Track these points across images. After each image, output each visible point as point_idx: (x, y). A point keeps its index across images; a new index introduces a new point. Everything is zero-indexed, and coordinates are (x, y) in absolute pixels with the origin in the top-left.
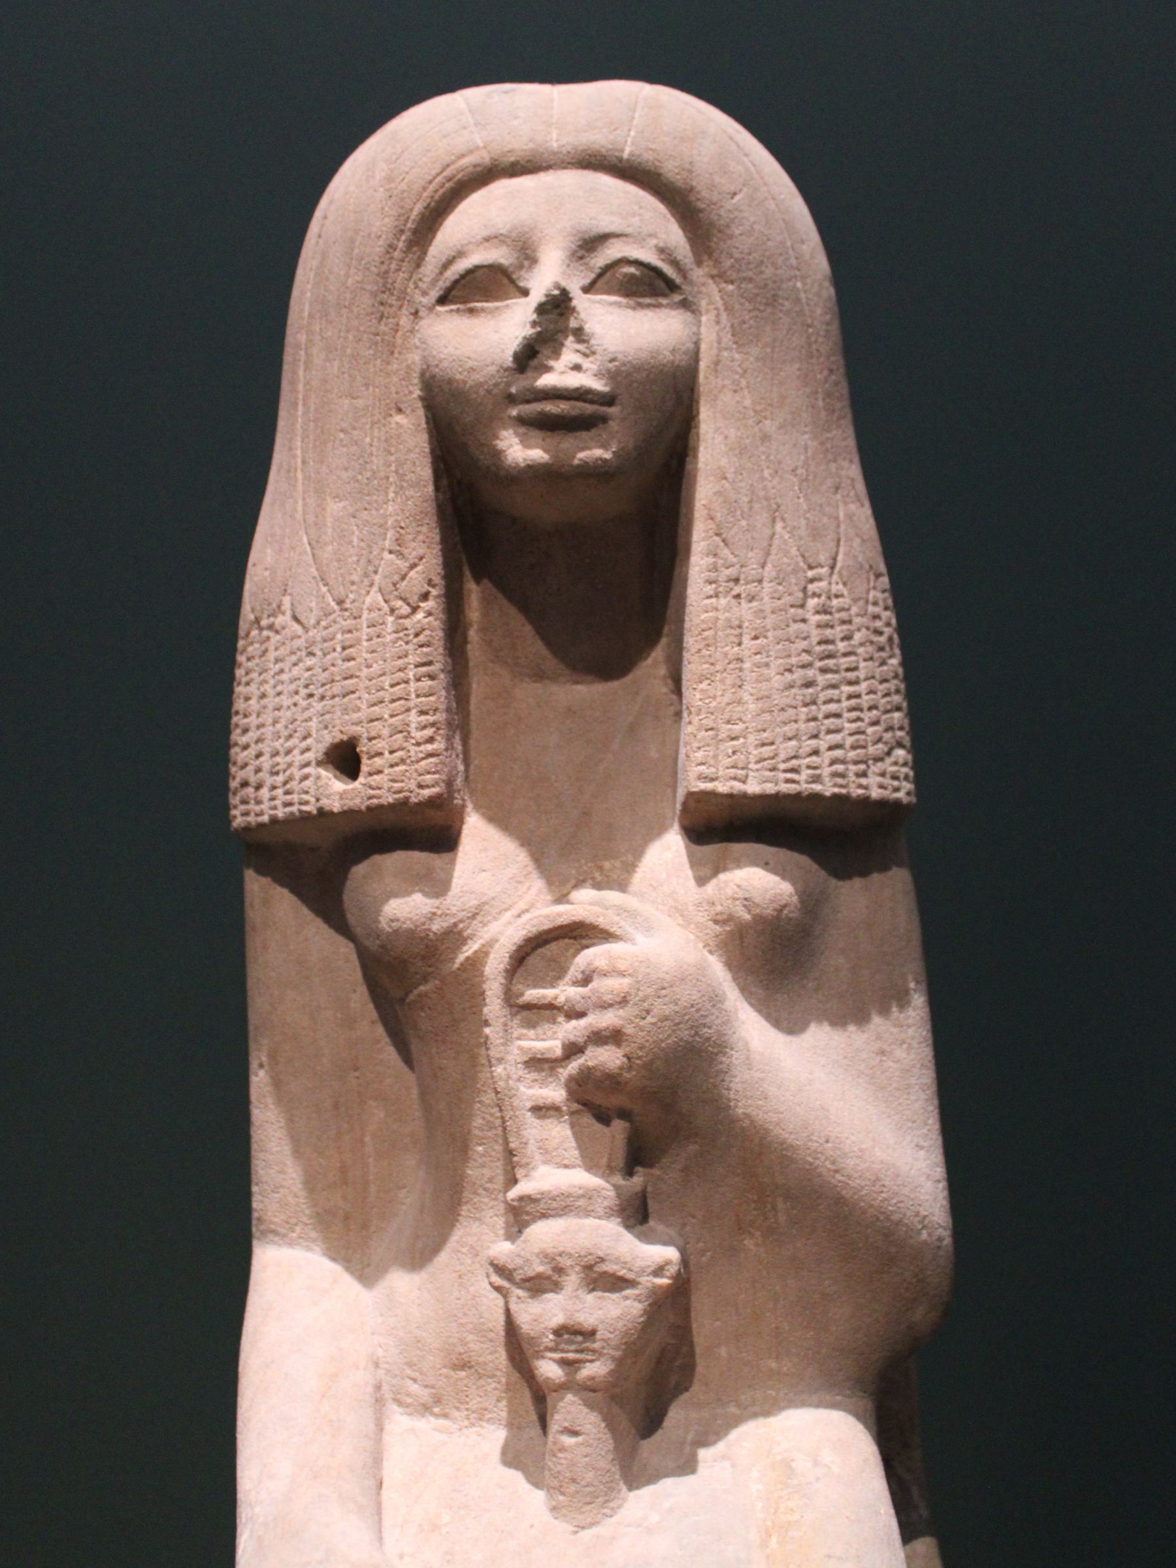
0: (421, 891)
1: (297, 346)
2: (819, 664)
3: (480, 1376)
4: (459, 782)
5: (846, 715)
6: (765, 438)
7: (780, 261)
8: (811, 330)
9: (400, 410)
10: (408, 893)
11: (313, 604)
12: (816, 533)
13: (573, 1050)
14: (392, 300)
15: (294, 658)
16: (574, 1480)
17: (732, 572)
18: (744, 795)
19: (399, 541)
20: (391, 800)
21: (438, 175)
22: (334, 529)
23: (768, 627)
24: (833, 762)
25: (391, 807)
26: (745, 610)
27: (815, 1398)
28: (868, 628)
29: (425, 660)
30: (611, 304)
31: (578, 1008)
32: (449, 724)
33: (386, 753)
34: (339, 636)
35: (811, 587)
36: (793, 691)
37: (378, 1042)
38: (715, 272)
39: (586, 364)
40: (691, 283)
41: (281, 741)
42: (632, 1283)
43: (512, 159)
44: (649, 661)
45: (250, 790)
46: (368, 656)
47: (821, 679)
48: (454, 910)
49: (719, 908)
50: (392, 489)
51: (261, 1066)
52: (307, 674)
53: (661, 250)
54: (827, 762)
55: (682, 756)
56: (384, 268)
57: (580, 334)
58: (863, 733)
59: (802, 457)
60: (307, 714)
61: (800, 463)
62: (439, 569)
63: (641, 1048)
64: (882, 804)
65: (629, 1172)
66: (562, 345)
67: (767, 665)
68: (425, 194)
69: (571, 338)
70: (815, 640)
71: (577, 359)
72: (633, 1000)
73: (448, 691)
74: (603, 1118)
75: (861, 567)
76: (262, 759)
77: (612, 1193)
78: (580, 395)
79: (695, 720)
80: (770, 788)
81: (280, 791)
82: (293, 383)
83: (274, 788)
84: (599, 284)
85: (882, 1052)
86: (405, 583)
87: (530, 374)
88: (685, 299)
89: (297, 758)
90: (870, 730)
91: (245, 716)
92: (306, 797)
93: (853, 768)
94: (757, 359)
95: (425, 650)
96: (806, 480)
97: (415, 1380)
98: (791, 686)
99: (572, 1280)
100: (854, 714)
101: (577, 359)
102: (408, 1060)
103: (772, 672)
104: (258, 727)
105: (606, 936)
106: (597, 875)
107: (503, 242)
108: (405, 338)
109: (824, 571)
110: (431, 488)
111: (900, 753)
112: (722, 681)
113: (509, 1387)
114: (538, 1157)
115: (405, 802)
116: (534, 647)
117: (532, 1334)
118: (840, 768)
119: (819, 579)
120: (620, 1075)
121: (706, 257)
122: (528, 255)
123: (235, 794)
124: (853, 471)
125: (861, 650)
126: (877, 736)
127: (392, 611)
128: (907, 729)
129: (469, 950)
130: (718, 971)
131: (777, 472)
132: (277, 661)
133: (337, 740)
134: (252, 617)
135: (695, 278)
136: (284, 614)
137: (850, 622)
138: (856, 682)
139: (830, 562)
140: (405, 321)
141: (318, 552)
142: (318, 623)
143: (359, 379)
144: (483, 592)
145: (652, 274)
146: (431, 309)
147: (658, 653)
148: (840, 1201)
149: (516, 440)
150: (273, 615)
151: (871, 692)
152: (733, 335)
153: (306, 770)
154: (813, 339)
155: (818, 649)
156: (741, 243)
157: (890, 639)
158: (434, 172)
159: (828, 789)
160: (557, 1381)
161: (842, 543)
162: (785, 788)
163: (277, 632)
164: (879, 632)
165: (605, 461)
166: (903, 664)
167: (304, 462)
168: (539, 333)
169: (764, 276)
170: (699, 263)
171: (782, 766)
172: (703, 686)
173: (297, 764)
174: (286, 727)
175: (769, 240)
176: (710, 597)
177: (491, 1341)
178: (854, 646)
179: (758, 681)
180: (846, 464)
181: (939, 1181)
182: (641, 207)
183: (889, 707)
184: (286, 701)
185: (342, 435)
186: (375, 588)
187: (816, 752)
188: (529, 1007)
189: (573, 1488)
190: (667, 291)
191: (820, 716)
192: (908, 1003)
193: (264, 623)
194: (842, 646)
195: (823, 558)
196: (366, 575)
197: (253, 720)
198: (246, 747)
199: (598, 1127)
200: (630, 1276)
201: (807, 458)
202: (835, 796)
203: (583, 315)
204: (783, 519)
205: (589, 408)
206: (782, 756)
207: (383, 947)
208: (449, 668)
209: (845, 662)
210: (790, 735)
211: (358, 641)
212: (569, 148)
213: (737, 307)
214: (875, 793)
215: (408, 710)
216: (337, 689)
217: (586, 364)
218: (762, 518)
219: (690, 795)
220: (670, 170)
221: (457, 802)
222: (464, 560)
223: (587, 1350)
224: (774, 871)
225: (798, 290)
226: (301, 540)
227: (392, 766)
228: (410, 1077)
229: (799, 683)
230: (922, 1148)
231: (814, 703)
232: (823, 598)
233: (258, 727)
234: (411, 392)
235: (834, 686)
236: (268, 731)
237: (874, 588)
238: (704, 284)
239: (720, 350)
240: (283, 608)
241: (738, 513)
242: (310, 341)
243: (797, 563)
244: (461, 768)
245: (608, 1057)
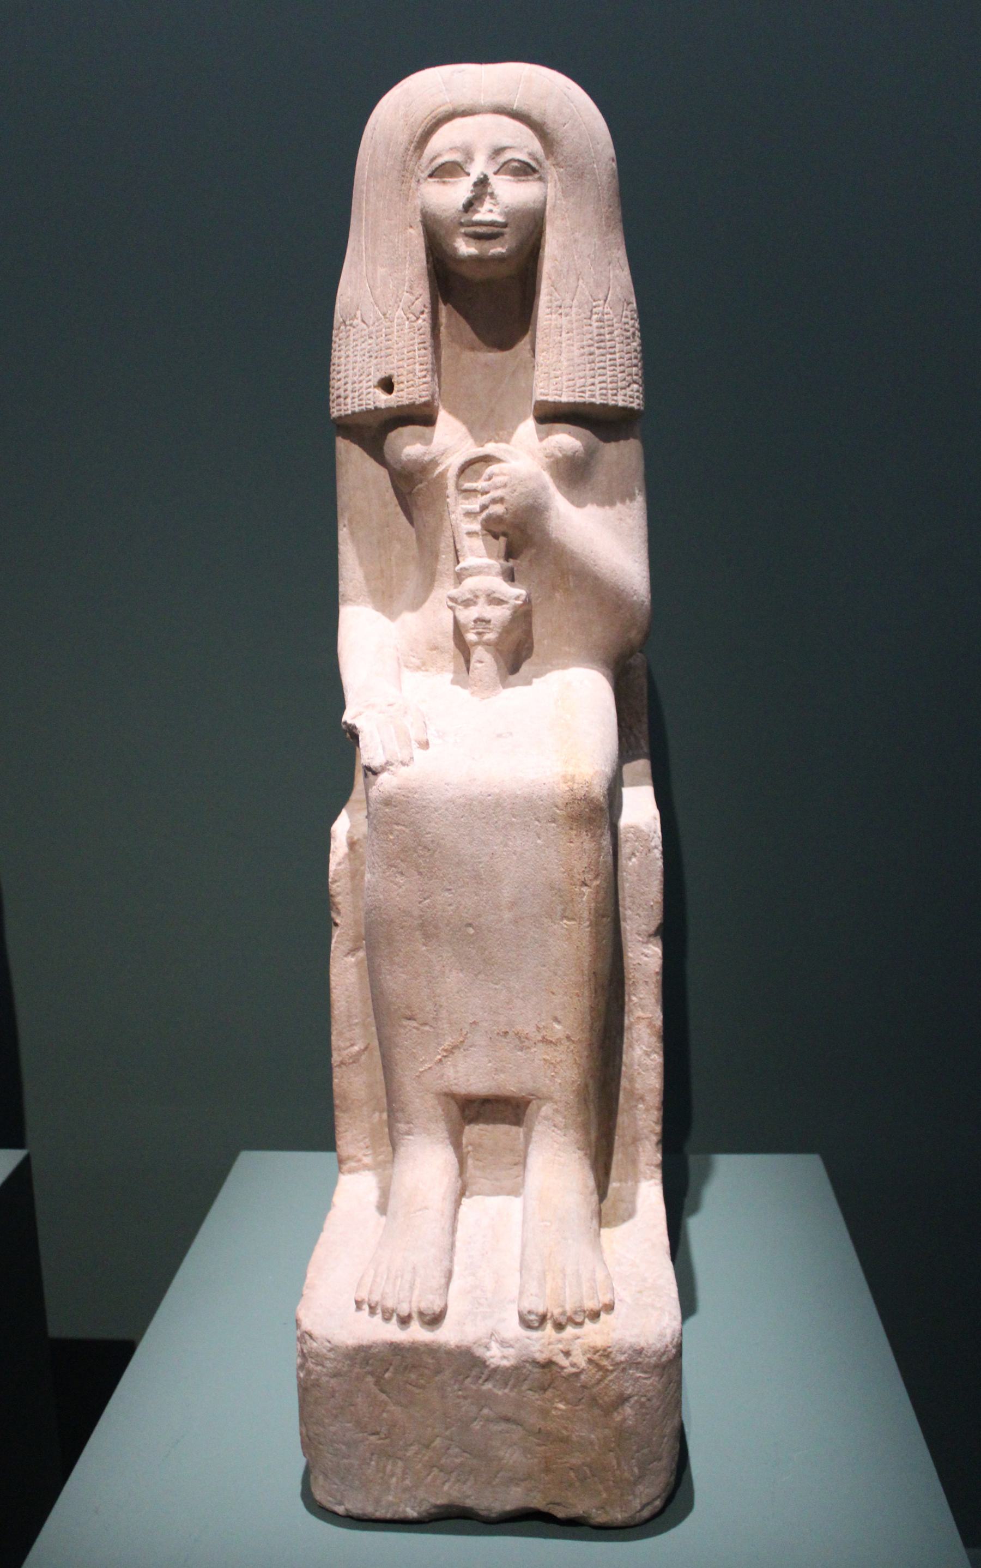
0: (421, 443)
1: (362, 192)
2: (596, 345)
3: (442, 652)
4: (436, 395)
5: (608, 368)
6: (576, 241)
7: (586, 155)
8: (600, 188)
9: (411, 227)
10: (415, 444)
11: (372, 315)
12: (598, 285)
13: (484, 507)
14: (408, 175)
15: (363, 340)
16: (481, 680)
17: (558, 303)
18: (560, 403)
19: (411, 287)
20: (407, 403)
21: (429, 115)
22: (381, 281)
23: (574, 328)
24: (601, 389)
25: (408, 406)
26: (564, 320)
27: (586, 664)
28: (621, 329)
29: (422, 341)
30: (507, 180)
31: (486, 490)
32: (433, 370)
33: (405, 382)
34: (384, 330)
35: (594, 310)
36: (584, 357)
37: (397, 514)
38: (554, 163)
39: (495, 209)
40: (544, 168)
41: (357, 377)
42: (506, 602)
43: (463, 109)
44: (523, 342)
45: (342, 400)
46: (397, 339)
47: (597, 352)
48: (434, 451)
49: (548, 451)
50: (408, 263)
51: (345, 526)
52: (369, 347)
53: (530, 154)
54: (598, 388)
55: (534, 385)
56: (404, 159)
57: (492, 195)
58: (616, 376)
59: (593, 249)
60: (369, 365)
61: (591, 253)
62: (429, 301)
63: (512, 505)
64: (624, 409)
65: (507, 559)
66: (484, 200)
67: (573, 345)
68: (423, 125)
69: (488, 197)
70: (595, 335)
71: (491, 207)
72: (509, 485)
73: (432, 355)
74: (496, 537)
75: (620, 300)
76: (347, 385)
77: (499, 566)
78: (492, 224)
79: (540, 369)
80: (572, 400)
81: (356, 400)
82: (360, 208)
83: (353, 398)
84: (501, 170)
85: (621, 519)
86: (413, 306)
87: (470, 213)
88: (541, 177)
89: (364, 384)
90: (620, 375)
91: (339, 366)
92: (369, 402)
93: (610, 392)
94: (573, 204)
95: (423, 336)
96: (595, 260)
97: (414, 657)
98: (583, 355)
99: (482, 600)
100: (612, 368)
101: (491, 207)
102: (412, 523)
103: (575, 348)
104: (345, 371)
105: (498, 460)
106: (497, 438)
107: (458, 150)
108: (414, 193)
109: (601, 302)
110: (425, 262)
111: (635, 386)
112: (552, 352)
113: (454, 657)
116: (470, 335)
117: (465, 623)
118: (604, 391)
119: (599, 306)
120: (503, 516)
121: (550, 155)
122: (469, 157)
123: (333, 402)
124: (621, 254)
125: (617, 339)
126: (623, 378)
127: (408, 319)
128: (640, 375)
129: (440, 469)
130: (547, 477)
131: (580, 257)
132: (354, 340)
133: (383, 377)
134: (341, 320)
135: (545, 166)
136: (357, 319)
137: (613, 326)
138: (614, 353)
139: (605, 298)
140: (413, 184)
141: (373, 291)
142: (374, 323)
143: (392, 211)
144: (447, 309)
145: (525, 166)
146: (426, 179)
147: (527, 339)
148: (596, 578)
149: (463, 243)
150: (352, 319)
151: (621, 358)
152: (562, 193)
153: (369, 390)
154: (601, 191)
155: (596, 338)
156: (567, 148)
157: (634, 334)
158: (427, 114)
159: (598, 400)
160: (475, 641)
161: (611, 289)
162: (579, 400)
163: (354, 327)
164: (628, 331)
165: (503, 253)
166: (642, 345)
167: (366, 248)
168: (474, 196)
169: (578, 164)
170: (547, 158)
171: (577, 390)
172: (544, 354)
173: (364, 387)
174: (359, 371)
175: (581, 145)
176: (548, 314)
177: (447, 637)
178: (614, 337)
179: (568, 352)
180: (615, 251)
181: (644, 578)
182: (521, 133)
183: (630, 365)
184: (359, 359)
185: (384, 237)
186: (400, 309)
187: (593, 384)
188: (466, 491)
189: (480, 683)
190: (532, 173)
191: (596, 368)
192: (635, 499)
193: (348, 323)
194: (608, 337)
195: (601, 296)
196: (396, 302)
197: (342, 368)
198: (339, 380)
199: (494, 541)
200: (505, 599)
201: (595, 250)
203: (494, 186)
204: (583, 279)
205: (496, 230)
206: (578, 385)
207: (402, 467)
208: (433, 345)
209: (609, 344)
210: (582, 376)
211: (393, 332)
212: (489, 104)
213: (564, 179)
214: (621, 404)
215: (415, 363)
216: (383, 353)
217: (495, 209)
218: (572, 279)
219: (537, 402)
220: (535, 115)
221: (436, 404)
222: (439, 294)
223: (487, 628)
224: (574, 436)
225: (595, 169)
226: (365, 285)
227: (408, 388)
228: (412, 530)
229: (587, 353)
230: (636, 562)
231: (593, 362)
232: (600, 315)
233: (345, 371)
234: (416, 218)
235: (603, 355)
236: (350, 372)
237: (626, 310)
238: (550, 168)
239: (556, 200)
240: (357, 316)
241: (562, 276)
242: (368, 190)
243: (588, 299)
244: (437, 389)
245: (498, 509)
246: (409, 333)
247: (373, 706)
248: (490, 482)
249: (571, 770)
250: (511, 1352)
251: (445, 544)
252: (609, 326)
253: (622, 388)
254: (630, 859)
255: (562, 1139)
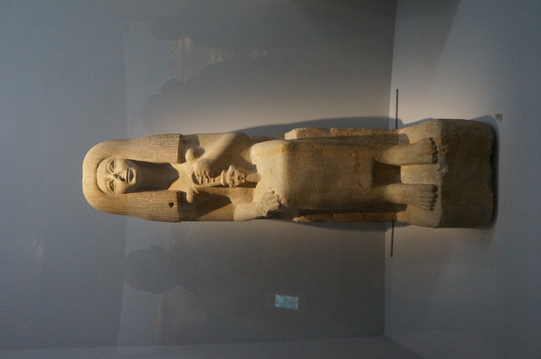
13: (207, 177)
17: (150, 156)
18: (178, 156)
19: (144, 197)
26: (155, 154)
47: (164, 145)
70: (159, 146)
71: (123, 174)
80: (177, 152)
93: (175, 142)
99: (233, 178)
109: (150, 144)
114: (220, 182)
115: (177, 197)
122: (108, 179)
127: (153, 198)
130: (199, 160)
132: (158, 214)
138: (164, 141)
146: (114, 192)
151: (166, 139)
153: (173, 210)
155: (160, 146)
159: (177, 145)
186: (150, 201)
187: (173, 147)
193: (153, 216)
194: (160, 142)
195: (148, 144)
202: (178, 144)
205: (129, 172)
214: (178, 139)
216: (162, 206)
220: (98, 161)
245: (207, 173)
246: (157, 198)
247: (262, 207)
248: (200, 175)
249: (281, 150)
250: (444, 166)
251: (217, 191)
252: (157, 142)
253: (174, 139)
254: (306, 136)
255: (385, 154)
